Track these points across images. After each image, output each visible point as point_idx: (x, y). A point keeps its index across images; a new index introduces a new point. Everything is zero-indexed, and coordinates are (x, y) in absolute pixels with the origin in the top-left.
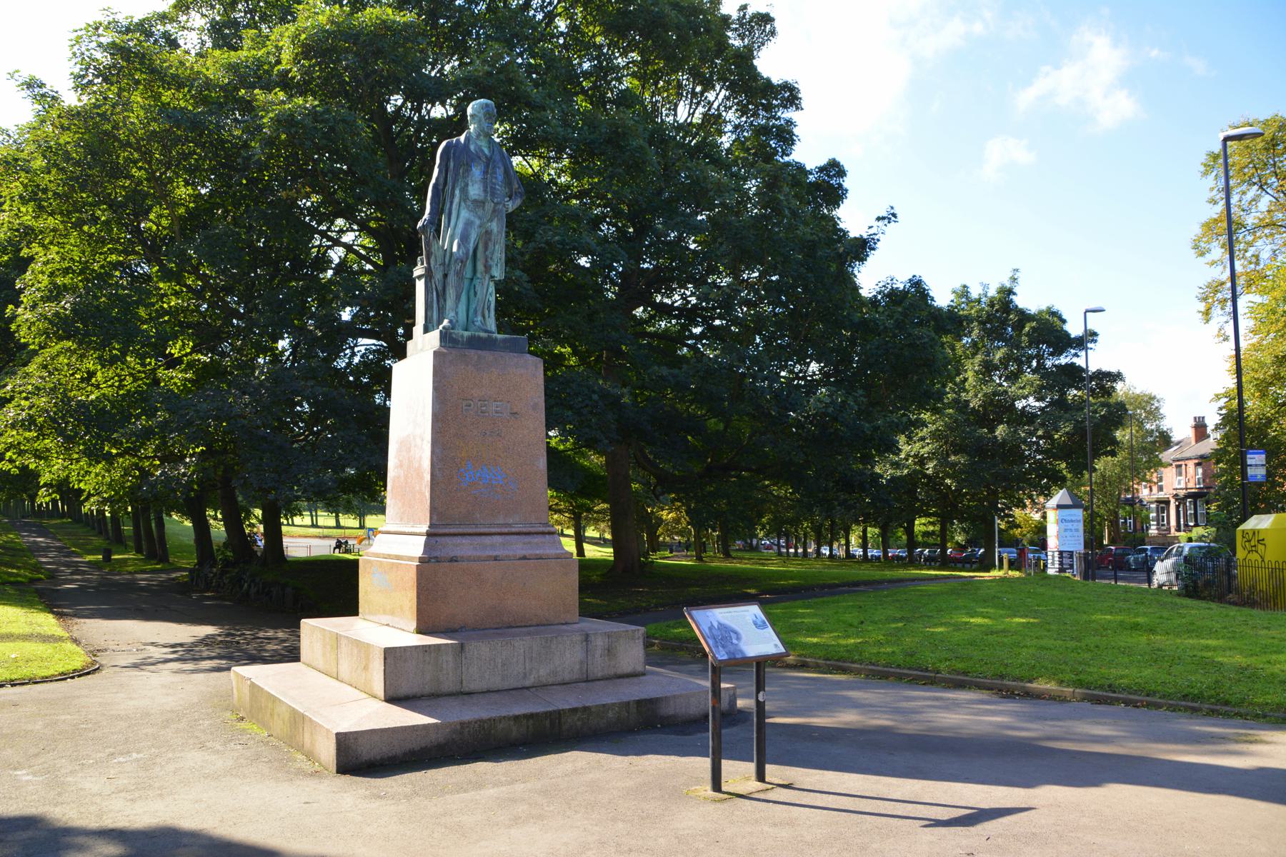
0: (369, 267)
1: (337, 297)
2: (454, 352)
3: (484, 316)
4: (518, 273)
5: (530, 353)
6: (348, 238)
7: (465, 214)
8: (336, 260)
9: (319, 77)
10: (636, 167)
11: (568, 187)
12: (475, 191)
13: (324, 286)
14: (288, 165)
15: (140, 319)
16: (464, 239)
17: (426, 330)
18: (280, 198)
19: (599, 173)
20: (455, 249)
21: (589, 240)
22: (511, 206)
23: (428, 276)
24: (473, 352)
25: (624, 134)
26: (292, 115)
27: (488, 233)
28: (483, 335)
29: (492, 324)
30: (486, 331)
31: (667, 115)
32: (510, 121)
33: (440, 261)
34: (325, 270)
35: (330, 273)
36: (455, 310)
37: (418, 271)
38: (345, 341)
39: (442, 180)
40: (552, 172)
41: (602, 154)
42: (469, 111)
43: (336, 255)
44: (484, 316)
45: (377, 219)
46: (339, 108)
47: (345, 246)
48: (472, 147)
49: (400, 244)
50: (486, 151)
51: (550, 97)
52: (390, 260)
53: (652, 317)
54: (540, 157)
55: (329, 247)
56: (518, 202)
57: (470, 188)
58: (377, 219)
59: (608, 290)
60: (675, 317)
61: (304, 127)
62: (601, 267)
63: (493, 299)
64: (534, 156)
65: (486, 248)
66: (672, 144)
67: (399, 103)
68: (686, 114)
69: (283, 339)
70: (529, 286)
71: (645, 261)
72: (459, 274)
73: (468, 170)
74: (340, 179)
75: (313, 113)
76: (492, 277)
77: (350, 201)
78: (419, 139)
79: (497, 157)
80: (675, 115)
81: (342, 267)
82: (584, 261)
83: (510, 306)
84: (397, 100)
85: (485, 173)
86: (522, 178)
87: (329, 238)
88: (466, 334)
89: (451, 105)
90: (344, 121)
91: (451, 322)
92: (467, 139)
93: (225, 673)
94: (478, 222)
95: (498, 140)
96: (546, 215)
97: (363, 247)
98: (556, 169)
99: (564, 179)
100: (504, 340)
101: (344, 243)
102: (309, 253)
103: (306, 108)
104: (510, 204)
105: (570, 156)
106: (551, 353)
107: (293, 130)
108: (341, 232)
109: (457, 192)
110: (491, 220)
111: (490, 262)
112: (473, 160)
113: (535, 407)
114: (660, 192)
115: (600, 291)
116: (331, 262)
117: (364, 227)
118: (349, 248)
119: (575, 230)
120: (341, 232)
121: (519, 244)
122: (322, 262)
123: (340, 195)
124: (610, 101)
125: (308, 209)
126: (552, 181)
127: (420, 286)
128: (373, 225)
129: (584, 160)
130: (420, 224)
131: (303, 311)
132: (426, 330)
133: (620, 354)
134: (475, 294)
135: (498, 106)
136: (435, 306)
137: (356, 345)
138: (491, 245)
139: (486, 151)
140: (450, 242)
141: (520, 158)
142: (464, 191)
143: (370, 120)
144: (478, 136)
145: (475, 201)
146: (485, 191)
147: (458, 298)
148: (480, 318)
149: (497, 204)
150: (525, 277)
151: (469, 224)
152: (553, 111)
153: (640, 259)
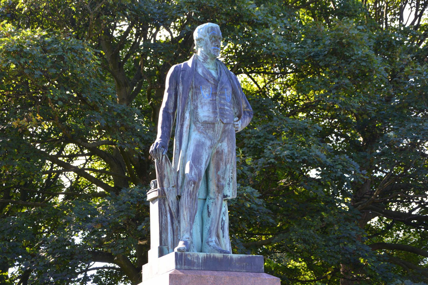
0: (100, 190)
1: (69, 222)
2: (190, 274)
3: (218, 236)
4: (249, 189)
5: (268, 270)
6: (79, 162)
7: (195, 136)
8: (68, 184)
9: (45, 8)
10: (362, 76)
11: (294, 101)
12: (205, 112)
13: (57, 210)
14: (18, 94)
15: (313, 260)
16: (196, 160)
17: (161, 253)
18: (10, 127)
19: (325, 84)
20: (187, 170)
21: (317, 151)
22: (241, 125)
23: (162, 198)
24: (209, 272)
25: (349, 44)
26: (21, 46)
27: (219, 153)
28: (218, 255)
29: (226, 243)
30: (221, 251)
31: (392, 20)
32: (234, 40)
33: (172, 183)
34: (57, 195)
35: (61, 197)
36: (189, 232)
37: (152, 194)
38: (75, 266)
39: (172, 104)
40: (277, 87)
41: (326, 66)
42: (196, 35)
43: (67, 179)
44: (218, 236)
45: (107, 143)
46: (67, 37)
47: (76, 169)
48: (200, 71)
49: (133, 168)
50: (214, 73)
51: (272, 13)
52: (121, 183)
53: (388, 227)
54: (264, 73)
55: (59, 172)
56: (247, 121)
57: (200, 110)
58: (107, 143)
59: (340, 201)
60: (414, 226)
61: (33, 57)
62: (331, 176)
63: (226, 219)
64: (259, 73)
65: (218, 168)
66: (399, 50)
67: (125, 29)
68: (413, 17)
69: (13, 266)
70: (260, 202)
71: (377, 169)
72: (192, 195)
73: (196, 94)
74: (70, 105)
75: (42, 45)
76: (225, 196)
77: (81, 126)
78: (146, 63)
79: (225, 78)
80: (401, 19)
81: (74, 192)
82: (313, 173)
83: (241, 219)
84: (123, 25)
85: (214, 94)
86: (248, 94)
87: (60, 164)
88: (201, 255)
89: (175, 28)
90: (72, 50)
91: (185, 243)
92: (195, 63)
94: (208, 143)
95: (222, 59)
96: (274, 130)
97: (94, 170)
98: (281, 83)
99: (290, 93)
100: (240, 260)
101: (78, 167)
102: (40, 180)
103: (34, 39)
104: (240, 123)
105: (295, 71)
106: (285, 268)
107: (22, 61)
108: (72, 157)
109: (187, 115)
110: (221, 141)
111: (223, 182)
112: (201, 83)
114: (389, 99)
115: (331, 202)
116: (63, 186)
117: (94, 151)
118: (80, 172)
119: (303, 144)
120: (72, 157)
121: (249, 161)
122: (53, 187)
123: (71, 121)
124: (333, 12)
125: (39, 136)
126: (278, 96)
127: (154, 209)
128: (102, 148)
129: (309, 73)
130: (152, 148)
131: (34, 236)
132: (161, 253)
133: (358, 267)
134: (209, 213)
135: (222, 27)
136: (169, 227)
137: (87, 270)
138: (222, 165)
139: (214, 73)
140: (183, 164)
141: (245, 76)
143: (98, 47)
144: (205, 59)
145: (205, 123)
146: (214, 112)
147: (192, 219)
148: (214, 238)
149: (227, 124)
150: (256, 194)
151: (200, 145)
152: (275, 27)
153: (371, 168)
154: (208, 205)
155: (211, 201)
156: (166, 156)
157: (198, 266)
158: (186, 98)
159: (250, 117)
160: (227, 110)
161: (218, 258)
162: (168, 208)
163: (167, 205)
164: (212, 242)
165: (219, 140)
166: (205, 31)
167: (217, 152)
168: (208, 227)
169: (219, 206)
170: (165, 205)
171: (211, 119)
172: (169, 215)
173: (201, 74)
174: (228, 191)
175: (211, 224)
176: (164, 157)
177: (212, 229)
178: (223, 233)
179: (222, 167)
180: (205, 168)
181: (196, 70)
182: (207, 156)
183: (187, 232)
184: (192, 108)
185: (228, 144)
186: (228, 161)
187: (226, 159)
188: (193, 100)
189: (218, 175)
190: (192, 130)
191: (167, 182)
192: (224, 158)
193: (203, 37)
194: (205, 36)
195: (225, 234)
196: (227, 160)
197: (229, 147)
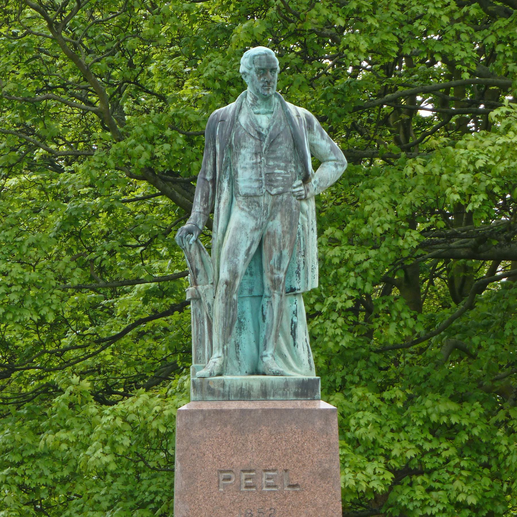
109: (225, 185)
134: (264, 317)
142: (233, 182)
154: (263, 308)
155: (266, 300)
160: (279, 174)
164: (266, 356)
165: (269, 218)
166: (250, 62)
168: (263, 335)
171: (252, 192)
172: (206, 323)
173: (243, 125)
174: (296, 282)
175: (267, 332)
177: (267, 338)
178: (294, 340)
181: (238, 117)
182: (249, 243)
185: (282, 222)
186: (284, 246)
187: (280, 242)
192: (277, 241)
195: (297, 341)
196: (282, 244)
197: (283, 226)
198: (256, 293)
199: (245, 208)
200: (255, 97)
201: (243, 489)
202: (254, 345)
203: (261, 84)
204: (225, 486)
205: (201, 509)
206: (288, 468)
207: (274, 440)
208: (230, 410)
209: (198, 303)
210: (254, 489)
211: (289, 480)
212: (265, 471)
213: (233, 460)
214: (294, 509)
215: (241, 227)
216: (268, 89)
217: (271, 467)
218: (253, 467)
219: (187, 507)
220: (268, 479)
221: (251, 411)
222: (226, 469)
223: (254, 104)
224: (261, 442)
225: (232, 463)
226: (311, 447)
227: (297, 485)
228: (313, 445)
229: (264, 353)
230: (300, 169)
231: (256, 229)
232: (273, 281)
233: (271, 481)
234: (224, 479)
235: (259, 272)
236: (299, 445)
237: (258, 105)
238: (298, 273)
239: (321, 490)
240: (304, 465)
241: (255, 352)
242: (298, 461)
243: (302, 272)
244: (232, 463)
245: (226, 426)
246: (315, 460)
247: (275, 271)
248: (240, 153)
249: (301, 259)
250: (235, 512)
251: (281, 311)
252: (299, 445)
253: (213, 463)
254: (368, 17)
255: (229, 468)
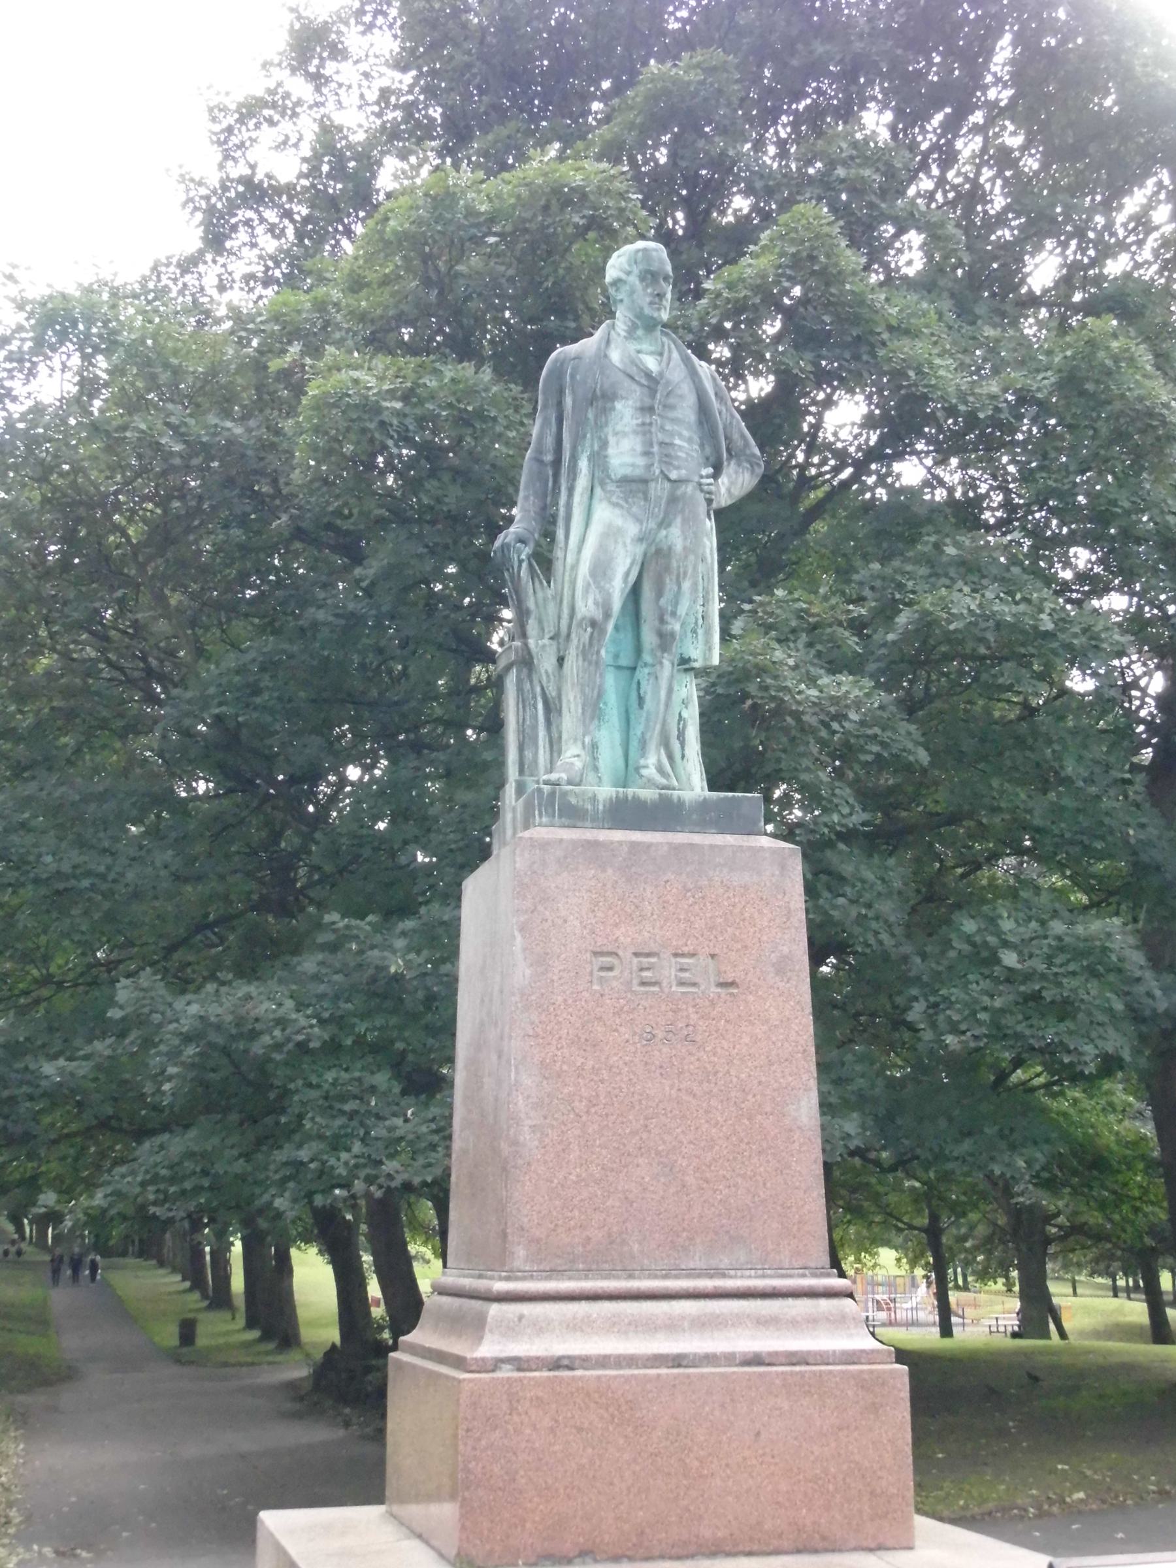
7: (604, 513)
57: (611, 451)
63: (692, 715)
72: (588, 653)
93: (826, 1260)
94: (633, 529)
109: (583, 464)
113: (782, 967)
134: (641, 700)
136: (542, 733)
138: (670, 585)
142: (599, 460)
145: (625, 481)
146: (647, 453)
154: (639, 683)
155: (646, 670)
156: (530, 565)
157: (593, 821)
158: (580, 424)
159: (753, 472)
161: (645, 802)
162: (538, 689)
163: (536, 682)
164: (646, 767)
167: (658, 552)
168: (639, 733)
169: (664, 684)
170: (531, 682)
171: (638, 472)
172: (540, 706)
175: (647, 727)
176: (525, 565)
177: (648, 736)
179: (668, 587)
180: (622, 590)
182: (628, 561)
183: (575, 740)
184: (596, 448)
185: (683, 532)
186: (685, 573)
188: (599, 426)
189: (660, 608)
190: (595, 502)
191: (536, 626)
192: (674, 564)
193: (623, 276)
194: (629, 273)
195: (686, 752)
198: (625, 661)
199: (622, 502)
200: (634, 323)
201: (636, 988)
202: (619, 752)
203: (648, 299)
204: (601, 980)
205: (559, 1023)
206: (717, 951)
207: (691, 900)
208: (612, 843)
209: (525, 671)
210: (656, 989)
211: (719, 973)
212: (676, 955)
213: (618, 933)
214: (729, 1027)
215: (611, 533)
216: (659, 309)
217: (686, 950)
218: (654, 947)
219: (534, 1017)
220: (681, 970)
221: (649, 846)
222: (605, 949)
223: (631, 334)
224: (667, 902)
225: (617, 940)
226: (756, 915)
227: (732, 984)
228: (760, 912)
229: (642, 762)
230: (708, 450)
231: (640, 540)
232: (661, 635)
233: (686, 975)
234: (602, 969)
235: (629, 628)
236: (737, 911)
237: (638, 339)
238: (694, 631)
239: (776, 993)
240: (746, 947)
241: (621, 763)
242: (734, 938)
243: (700, 631)
244: (617, 940)
245: (604, 871)
246: (765, 938)
247: (668, 618)
248: (613, 409)
249: (701, 609)
250: (622, 1029)
251: (670, 691)
252: (737, 911)
253: (583, 937)
254: (500, 539)
255: (610, 948)
